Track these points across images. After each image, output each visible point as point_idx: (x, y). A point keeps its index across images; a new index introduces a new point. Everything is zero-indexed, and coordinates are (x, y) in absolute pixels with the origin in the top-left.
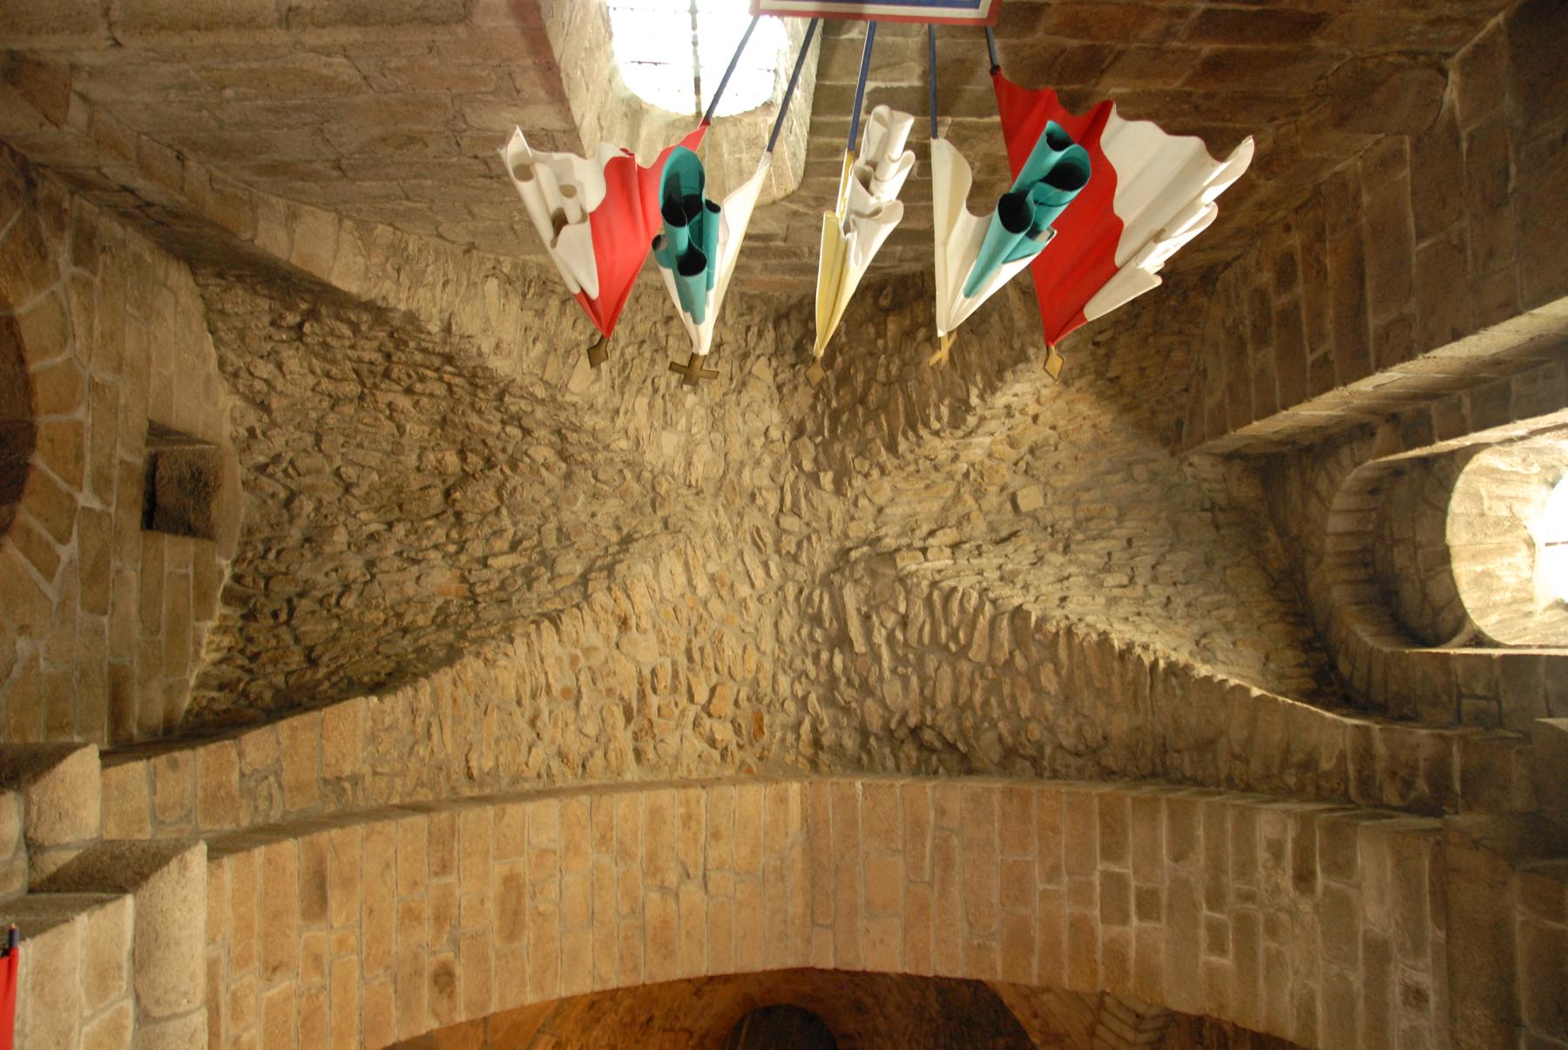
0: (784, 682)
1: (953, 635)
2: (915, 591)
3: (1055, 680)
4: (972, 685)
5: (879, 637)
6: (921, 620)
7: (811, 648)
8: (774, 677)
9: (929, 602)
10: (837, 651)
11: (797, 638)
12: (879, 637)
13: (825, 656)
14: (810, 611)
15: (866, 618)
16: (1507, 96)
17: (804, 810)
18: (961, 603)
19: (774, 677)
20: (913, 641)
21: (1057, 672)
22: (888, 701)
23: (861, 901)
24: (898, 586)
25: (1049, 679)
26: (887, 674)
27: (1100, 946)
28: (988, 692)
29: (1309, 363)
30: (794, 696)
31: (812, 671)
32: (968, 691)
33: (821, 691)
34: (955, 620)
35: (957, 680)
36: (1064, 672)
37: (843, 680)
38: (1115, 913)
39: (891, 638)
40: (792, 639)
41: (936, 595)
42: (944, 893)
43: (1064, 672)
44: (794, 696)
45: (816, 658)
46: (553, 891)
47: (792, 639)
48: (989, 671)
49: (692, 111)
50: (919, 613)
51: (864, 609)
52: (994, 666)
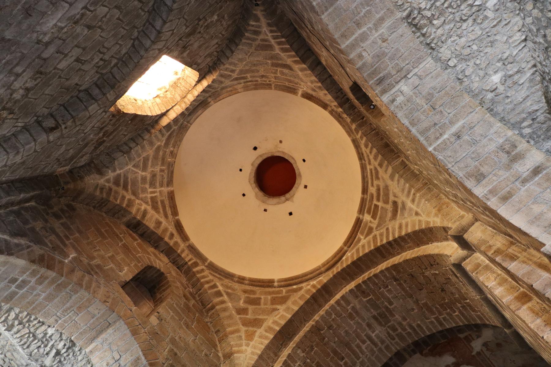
0: (80, 358)
1: (29, 337)
2: (29, 351)
3: (11, 314)
4: (34, 326)
5: (48, 349)
6: (34, 346)
7: (67, 358)
8: (81, 361)
9: (28, 347)
10: (61, 353)
11: (68, 363)
12: (48, 349)
13: (65, 355)
14: (60, 365)
15: (47, 354)
16: (146, 146)
17: (90, 344)
18: (20, 342)
19: (81, 361)
20: (40, 342)
21: (9, 315)
22: (59, 336)
23: (94, 319)
24: (33, 355)
25: (12, 315)
26: (54, 341)
27: (37, 277)
28: (32, 321)
29: (280, 76)
30: (80, 353)
31: (71, 354)
32: (37, 325)
33: (74, 348)
34: (25, 340)
35: (37, 328)
36: (6, 315)
37: (66, 347)
38: (24, 283)
39: (46, 346)
40: (70, 363)
41: (25, 347)
42: (71, 307)
43: (6, 315)
44: (80, 353)
45: (68, 356)
46: (425, 30)
47: (70, 363)
48: (27, 325)
49: (352, 83)
50: (33, 347)
51: (46, 356)
52: (24, 326)
